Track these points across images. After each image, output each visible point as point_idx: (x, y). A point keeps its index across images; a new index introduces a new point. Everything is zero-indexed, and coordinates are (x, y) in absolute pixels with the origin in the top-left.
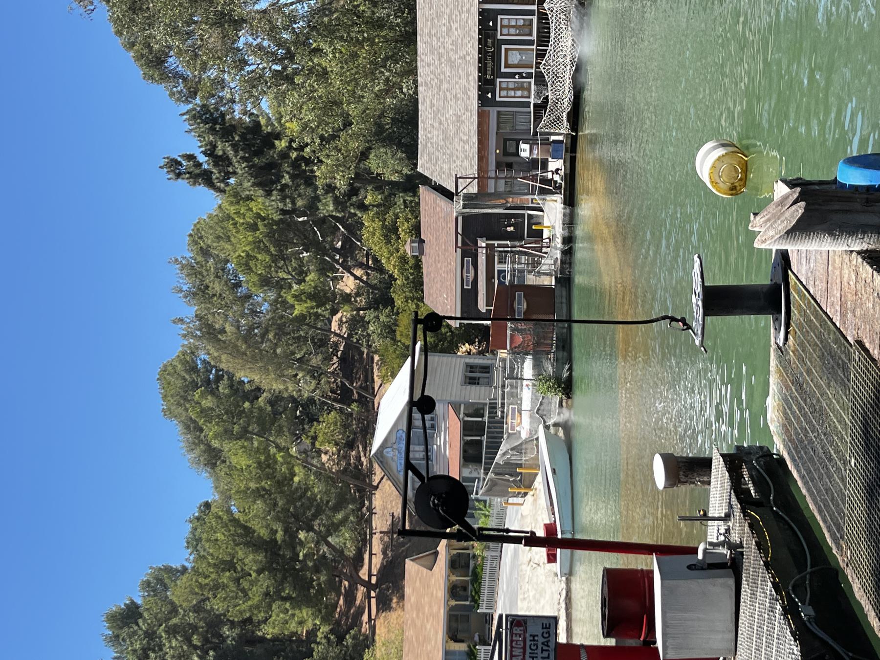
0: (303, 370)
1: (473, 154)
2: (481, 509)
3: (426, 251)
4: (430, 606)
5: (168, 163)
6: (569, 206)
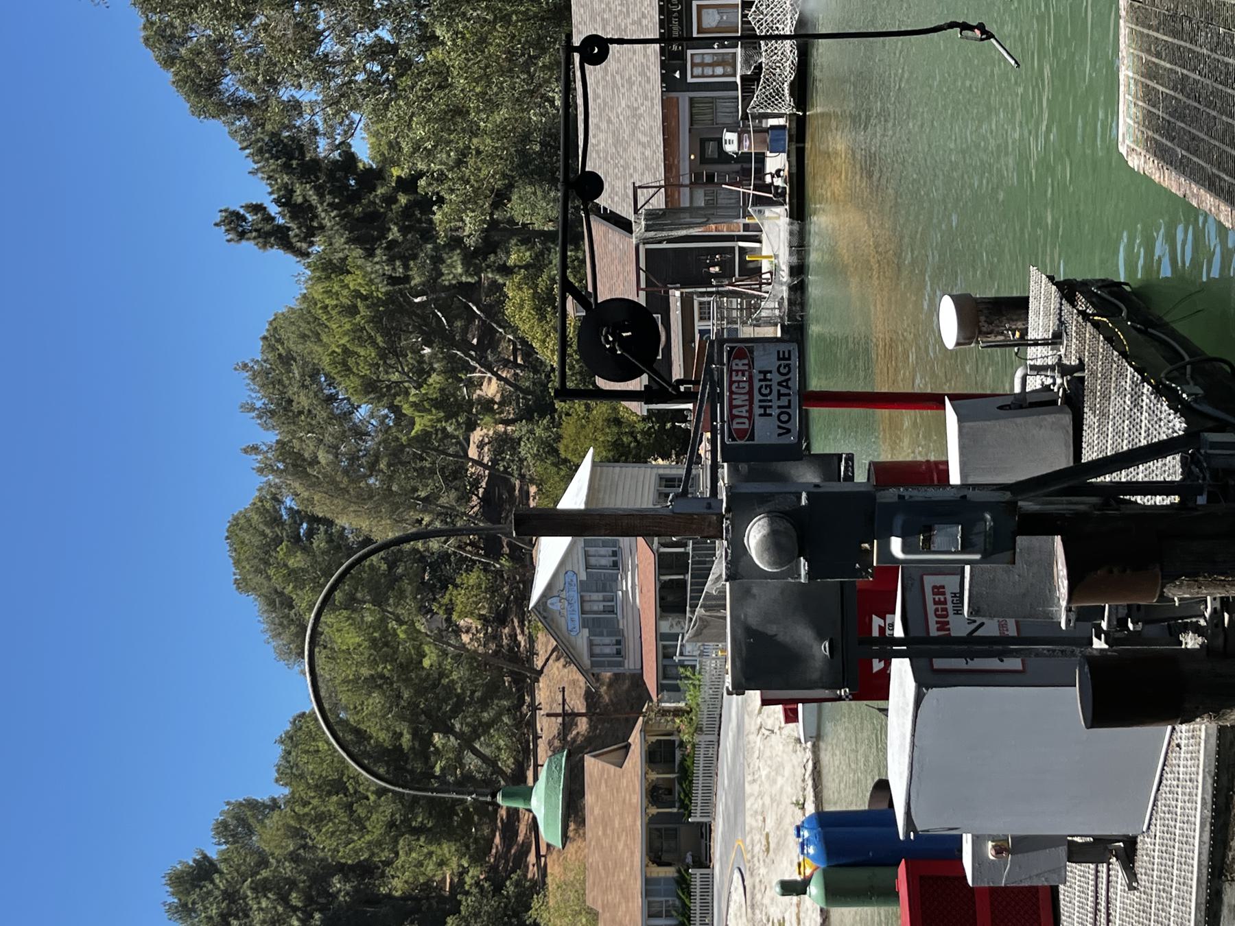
0: (430, 512)
1: (657, 162)
2: (687, 678)
4: (622, 818)
5: (226, 217)
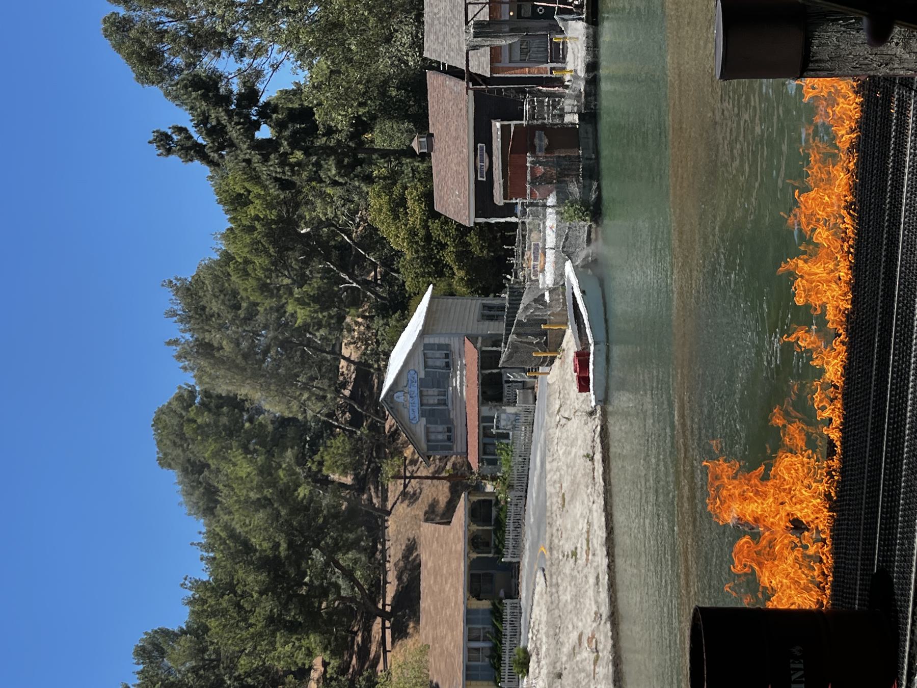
3: (436, 147)
5: (157, 137)
6: (592, 24)
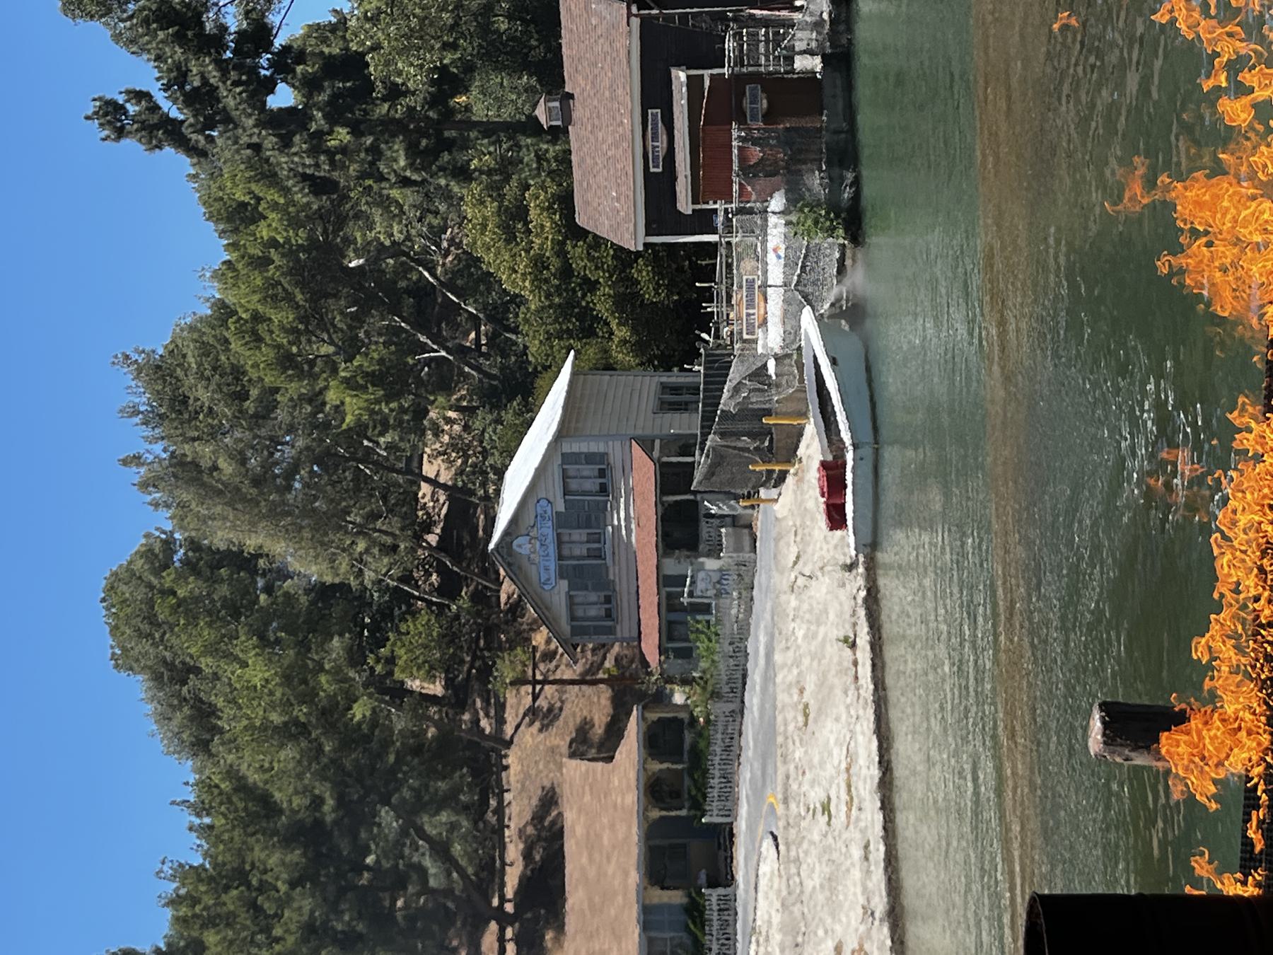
3: (575, 115)
